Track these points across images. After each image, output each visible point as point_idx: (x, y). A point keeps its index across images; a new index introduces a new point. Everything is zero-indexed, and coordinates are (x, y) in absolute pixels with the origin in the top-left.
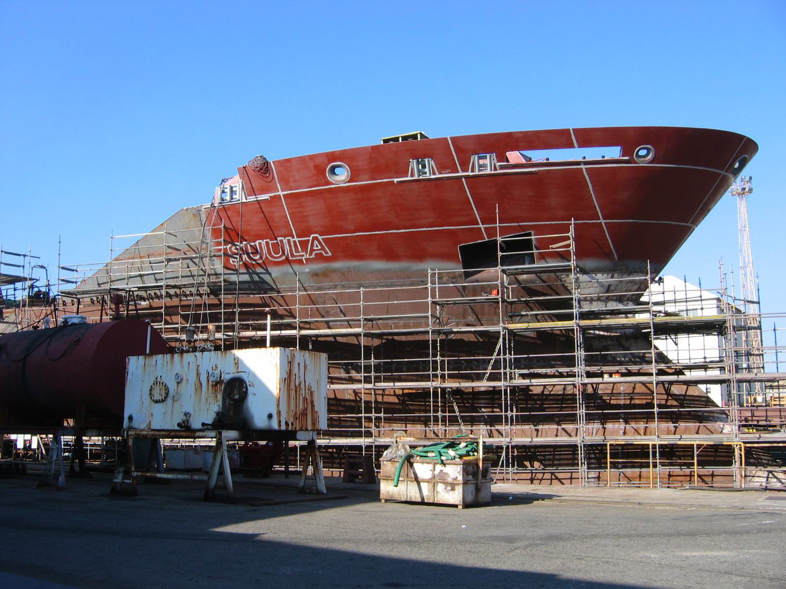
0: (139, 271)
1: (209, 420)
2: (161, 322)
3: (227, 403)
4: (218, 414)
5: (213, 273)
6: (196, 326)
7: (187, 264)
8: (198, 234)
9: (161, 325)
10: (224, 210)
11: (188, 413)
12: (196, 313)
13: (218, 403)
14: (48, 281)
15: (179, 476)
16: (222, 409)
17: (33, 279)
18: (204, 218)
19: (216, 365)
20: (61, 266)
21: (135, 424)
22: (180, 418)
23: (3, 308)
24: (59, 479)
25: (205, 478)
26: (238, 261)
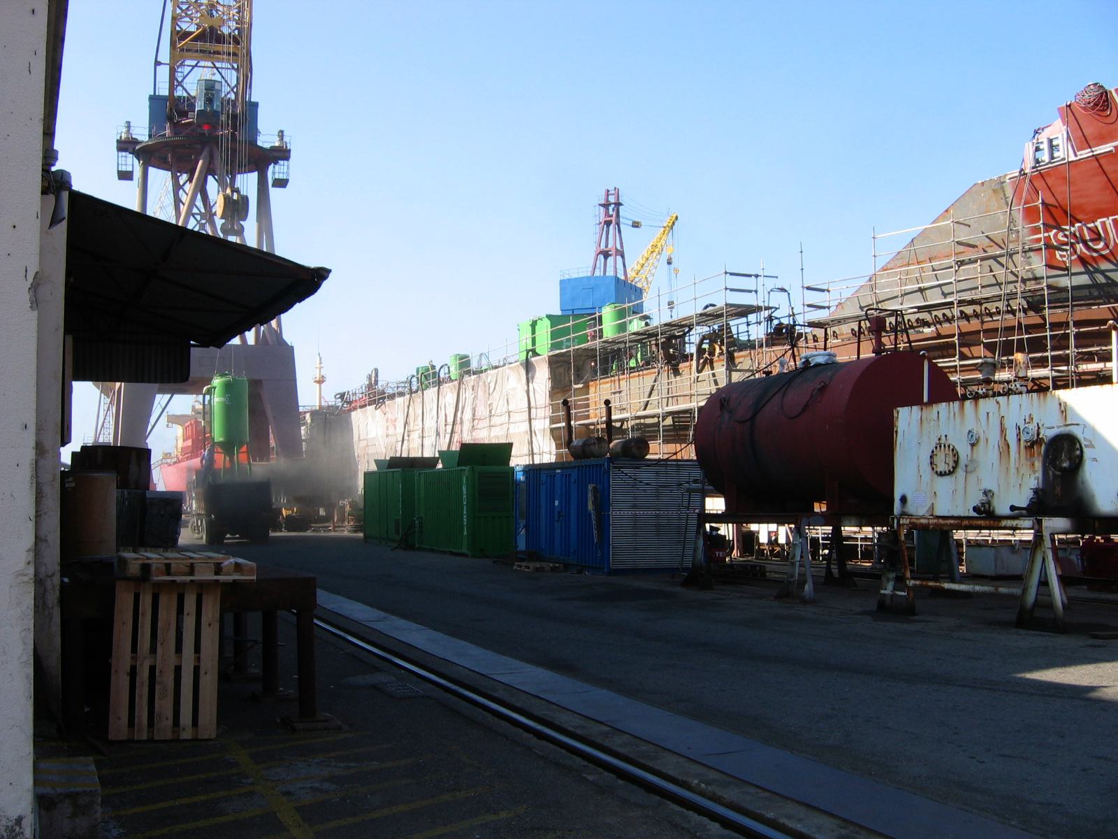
0: (918, 283)
1: (1023, 502)
2: (955, 357)
3: (1051, 473)
4: (1036, 491)
5: (1031, 277)
6: (1008, 359)
7: (990, 266)
8: (1003, 219)
9: (954, 361)
10: (1041, 177)
11: (990, 491)
12: (1007, 340)
13: (1037, 475)
14: (792, 308)
15: (978, 588)
16: (1043, 486)
17: (771, 308)
18: (1009, 192)
19: (1031, 414)
20: (805, 286)
21: (911, 508)
22: (976, 499)
23: (734, 351)
24: (804, 588)
25: (1016, 591)
26: (1068, 255)
